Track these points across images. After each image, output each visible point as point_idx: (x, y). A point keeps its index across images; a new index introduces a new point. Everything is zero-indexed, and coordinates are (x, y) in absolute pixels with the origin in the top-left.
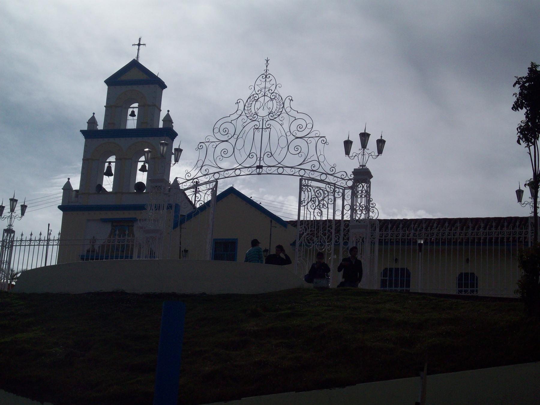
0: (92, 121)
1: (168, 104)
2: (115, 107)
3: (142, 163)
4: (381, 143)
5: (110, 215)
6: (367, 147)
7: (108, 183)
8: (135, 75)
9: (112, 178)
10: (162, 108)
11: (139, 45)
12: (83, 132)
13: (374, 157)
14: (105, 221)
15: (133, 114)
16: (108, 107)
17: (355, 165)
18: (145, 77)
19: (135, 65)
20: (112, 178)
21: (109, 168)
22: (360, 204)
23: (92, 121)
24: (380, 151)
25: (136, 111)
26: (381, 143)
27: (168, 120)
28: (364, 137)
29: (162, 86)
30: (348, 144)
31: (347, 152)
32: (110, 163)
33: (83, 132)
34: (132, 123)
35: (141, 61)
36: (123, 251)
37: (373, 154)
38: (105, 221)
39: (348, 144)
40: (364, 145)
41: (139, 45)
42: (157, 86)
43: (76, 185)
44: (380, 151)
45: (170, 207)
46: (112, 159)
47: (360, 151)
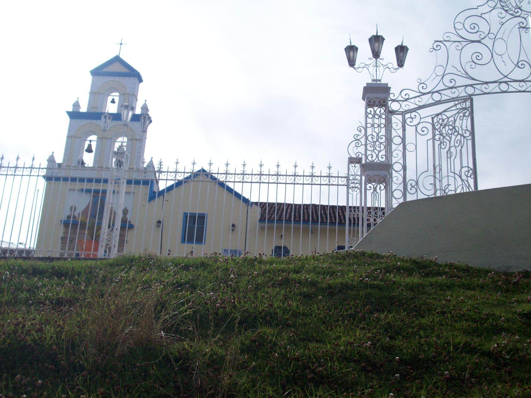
0: (77, 105)
1: (145, 95)
2: (97, 95)
3: (120, 144)
4: (401, 51)
5: (85, 186)
6: (381, 57)
7: (89, 159)
8: (117, 68)
9: (92, 155)
10: (139, 97)
11: (121, 44)
12: (69, 113)
13: (392, 69)
14: (88, 191)
15: (113, 101)
16: (93, 93)
17: (365, 78)
18: (126, 70)
19: (117, 59)
20: (92, 155)
21: (90, 146)
22: (378, 134)
23: (77, 105)
24: (401, 63)
25: (117, 100)
26: (401, 51)
27: (145, 108)
28: (376, 41)
29: (141, 80)
30: (351, 50)
31: (352, 63)
32: (91, 141)
33: (69, 113)
34: (112, 108)
35: (121, 56)
36: (94, 217)
37: (390, 66)
38: (88, 191)
39: (351, 50)
40: (376, 54)
41: (121, 44)
42: (136, 79)
43: (59, 159)
44: (401, 63)
45: (146, 183)
46: (94, 138)
47: (370, 61)
